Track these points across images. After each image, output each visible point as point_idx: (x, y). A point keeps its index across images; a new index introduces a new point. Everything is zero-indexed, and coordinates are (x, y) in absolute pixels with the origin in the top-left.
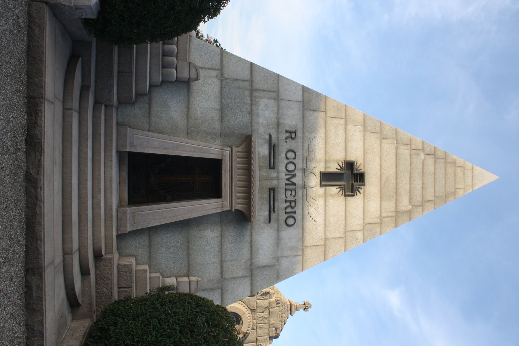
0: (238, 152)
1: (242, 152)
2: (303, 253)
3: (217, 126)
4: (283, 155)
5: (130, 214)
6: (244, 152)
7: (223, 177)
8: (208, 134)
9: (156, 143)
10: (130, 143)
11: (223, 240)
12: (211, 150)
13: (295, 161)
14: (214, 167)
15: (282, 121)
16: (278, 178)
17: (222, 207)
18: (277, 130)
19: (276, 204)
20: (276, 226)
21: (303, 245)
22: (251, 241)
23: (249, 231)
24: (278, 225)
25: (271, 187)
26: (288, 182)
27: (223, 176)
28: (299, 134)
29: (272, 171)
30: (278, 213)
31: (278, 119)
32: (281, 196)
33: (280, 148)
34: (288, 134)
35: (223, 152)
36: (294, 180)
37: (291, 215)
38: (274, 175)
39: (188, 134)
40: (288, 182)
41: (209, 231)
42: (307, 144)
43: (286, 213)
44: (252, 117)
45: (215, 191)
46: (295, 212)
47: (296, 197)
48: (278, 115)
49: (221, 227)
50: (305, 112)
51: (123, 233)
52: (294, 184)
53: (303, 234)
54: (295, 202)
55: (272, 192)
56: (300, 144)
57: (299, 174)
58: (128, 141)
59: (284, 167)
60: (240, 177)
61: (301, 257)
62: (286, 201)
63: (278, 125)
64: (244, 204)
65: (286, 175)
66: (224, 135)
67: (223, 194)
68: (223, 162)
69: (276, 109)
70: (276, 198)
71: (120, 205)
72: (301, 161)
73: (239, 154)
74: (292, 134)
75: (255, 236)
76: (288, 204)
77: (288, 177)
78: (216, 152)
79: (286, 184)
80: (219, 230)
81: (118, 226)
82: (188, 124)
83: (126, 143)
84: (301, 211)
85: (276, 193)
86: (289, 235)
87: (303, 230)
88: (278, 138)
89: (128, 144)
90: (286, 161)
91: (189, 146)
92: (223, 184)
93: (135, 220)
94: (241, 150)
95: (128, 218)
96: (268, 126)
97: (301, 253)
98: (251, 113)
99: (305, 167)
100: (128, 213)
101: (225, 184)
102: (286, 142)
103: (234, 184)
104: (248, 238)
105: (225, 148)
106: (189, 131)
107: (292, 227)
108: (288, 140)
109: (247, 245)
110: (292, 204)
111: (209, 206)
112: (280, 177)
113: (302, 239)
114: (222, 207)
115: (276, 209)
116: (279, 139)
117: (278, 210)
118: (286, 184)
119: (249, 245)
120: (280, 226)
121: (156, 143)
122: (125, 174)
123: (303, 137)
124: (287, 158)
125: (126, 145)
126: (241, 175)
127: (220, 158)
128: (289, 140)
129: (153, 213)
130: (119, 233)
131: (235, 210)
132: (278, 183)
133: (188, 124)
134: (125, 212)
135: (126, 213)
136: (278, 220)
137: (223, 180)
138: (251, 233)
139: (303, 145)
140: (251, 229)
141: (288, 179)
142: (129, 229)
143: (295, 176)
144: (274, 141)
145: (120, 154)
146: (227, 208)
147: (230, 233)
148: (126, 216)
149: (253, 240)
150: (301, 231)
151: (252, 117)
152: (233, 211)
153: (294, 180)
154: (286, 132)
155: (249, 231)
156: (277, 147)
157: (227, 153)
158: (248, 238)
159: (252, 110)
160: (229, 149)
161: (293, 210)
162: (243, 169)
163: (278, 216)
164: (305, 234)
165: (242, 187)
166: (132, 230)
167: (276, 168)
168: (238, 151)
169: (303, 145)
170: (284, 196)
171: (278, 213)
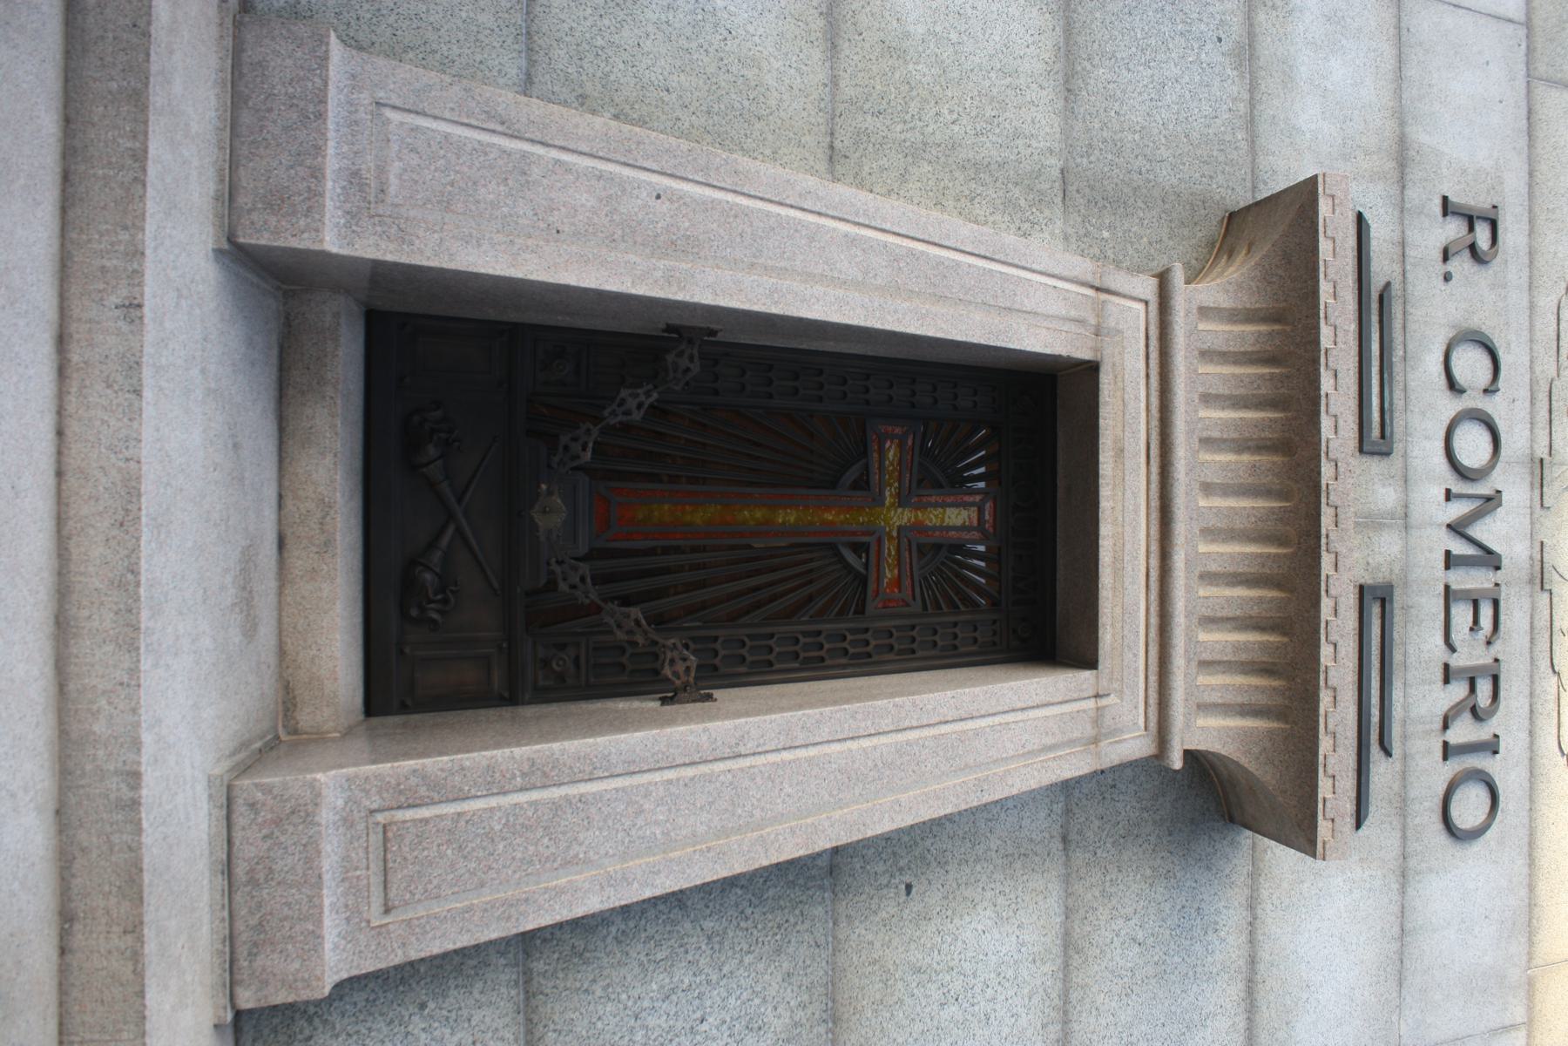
0: (1204, 312)
1: (1234, 316)
2: (1530, 1009)
3: (1038, 120)
4: (1432, 364)
5: (347, 822)
6: (1249, 316)
7: (1105, 504)
8: (976, 169)
9: (585, 199)
10: (354, 177)
11: (1077, 978)
12: (1011, 293)
13: (1495, 407)
14: (1025, 420)
15: (1423, 138)
16: (1404, 519)
17: (1095, 741)
18: (1394, 190)
19: (1397, 695)
20: (1392, 841)
21: (1530, 956)
22: (1253, 961)
23: (1238, 895)
24: (1404, 837)
25: (1368, 580)
26: (1460, 548)
27: (1105, 492)
28: (1513, 234)
29: (1375, 465)
30: (1405, 757)
31: (1401, 116)
32: (1420, 643)
33: (1416, 313)
34: (1454, 229)
35: (1100, 309)
36: (1484, 531)
37: (1472, 765)
38: (1386, 496)
39: (833, 155)
40: (1460, 548)
41: (984, 917)
42: (1554, 299)
43: (1447, 751)
44: (1253, 88)
45: (1033, 612)
46: (1491, 747)
47: (1497, 648)
48: (1398, 93)
49: (1067, 879)
50: (1540, 90)
51: (281, 997)
52: (1489, 558)
53: (1531, 888)
54: (1496, 679)
55: (1376, 610)
56: (1518, 298)
57: (1512, 484)
58: (332, 163)
59: (1439, 445)
60: (1232, 502)
61: (1522, 1034)
62: (1448, 675)
63: (1403, 157)
64: (1245, 710)
65: (1449, 495)
66: (1085, 192)
67: (1107, 637)
68: (1105, 380)
69: (1388, 51)
70: (1397, 657)
71: (281, 736)
72: (1523, 406)
73: (1218, 333)
74: (1476, 230)
75: (1273, 924)
76: (1458, 690)
77: (1458, 510)
78: (1056, 307)
79: (1450, 560)
80: (1053, 903)
81: (232, 938)
82: (834, 81)
83: (317, 174)
84: (1524, 736)
85: (1398, 618)
86: (1461, 886)
87: (1532, 862)
88: (1403, 244)
89: (331, 187)
90: (1450, 406)
91: (852, 241)
92: (1105, 556)
93: (396, 878)
94: (1225, 302)
95: (329, 863)
96: (1346, 157)
97: (1518, 1013)
98: (1247, 55)
99: (1541, 451)
100: (326, 816)
101: (1117, 559)
102: (1447, 278)
103: (1179, 559)
104: (1229, 947)
105: (1118, 280)
106: (843, 141)
107: (1477, 846)
108: (1454, 265)
109: (1226, 994)
110: (1479, 688)
111: (995, 730)
112: (1416, 515)
113: (1527, 920)
114: (1095, 741)
115: (1396, 731)
116: (1410, 252)
117: (1405, 737)
118: (1450, 560)
119: (1236, 991)
120: (1413, 846)
121: (585, 199)
122: (332, 475)
123: (1531, 254)
124: (1453, 385)
125: (315, 195)
126: (1227, 490)
127: (1084, 354)
128: (1461, 265)
129: (556, 807)
130: (248, 999)
131: (1188, 754)
132: (1406, 550)
133: (834, 81)
134: (303, 813)
135: (309, 819)
136: (1403, 806)
137: (1105, 530)
138: (1252, 905)
139: (1532, 306)
140: (1254, 875)
141: (1457, 529)
142: (336, 959)
143: (1491, 502)
144: (1382, 268)
145: (279, 287)
146: (1133, 744)
147: (1129, 910)
148: (311, 852)
149: (1264, 955)
150: (1521, 862)
151: (1253, 88)
152: (1177, 762)
153: (1484, 531)
154: (1447, 207)
155: (1238, 895)
156: (1397, 309)
157: (1131, 317)
158: (1229, 947)
159: (1251, 35)
160: (1146, 287)
161: (1482, 733)
162: (1241, 446)
163: (1404, 775)
164: (1542, 888)
165: (1236, 579)
166: (369, 966)
167: (1398, 447)
168: (1213, 302)
169: (1532, 306)
170: (1439, 639)
171: (1405, 757)
